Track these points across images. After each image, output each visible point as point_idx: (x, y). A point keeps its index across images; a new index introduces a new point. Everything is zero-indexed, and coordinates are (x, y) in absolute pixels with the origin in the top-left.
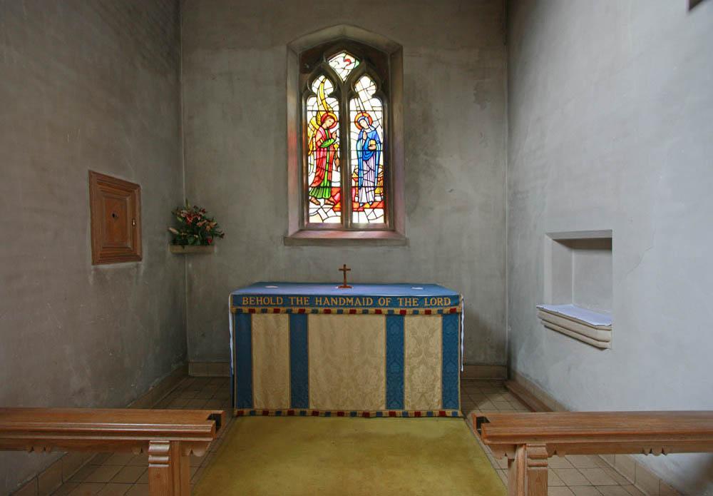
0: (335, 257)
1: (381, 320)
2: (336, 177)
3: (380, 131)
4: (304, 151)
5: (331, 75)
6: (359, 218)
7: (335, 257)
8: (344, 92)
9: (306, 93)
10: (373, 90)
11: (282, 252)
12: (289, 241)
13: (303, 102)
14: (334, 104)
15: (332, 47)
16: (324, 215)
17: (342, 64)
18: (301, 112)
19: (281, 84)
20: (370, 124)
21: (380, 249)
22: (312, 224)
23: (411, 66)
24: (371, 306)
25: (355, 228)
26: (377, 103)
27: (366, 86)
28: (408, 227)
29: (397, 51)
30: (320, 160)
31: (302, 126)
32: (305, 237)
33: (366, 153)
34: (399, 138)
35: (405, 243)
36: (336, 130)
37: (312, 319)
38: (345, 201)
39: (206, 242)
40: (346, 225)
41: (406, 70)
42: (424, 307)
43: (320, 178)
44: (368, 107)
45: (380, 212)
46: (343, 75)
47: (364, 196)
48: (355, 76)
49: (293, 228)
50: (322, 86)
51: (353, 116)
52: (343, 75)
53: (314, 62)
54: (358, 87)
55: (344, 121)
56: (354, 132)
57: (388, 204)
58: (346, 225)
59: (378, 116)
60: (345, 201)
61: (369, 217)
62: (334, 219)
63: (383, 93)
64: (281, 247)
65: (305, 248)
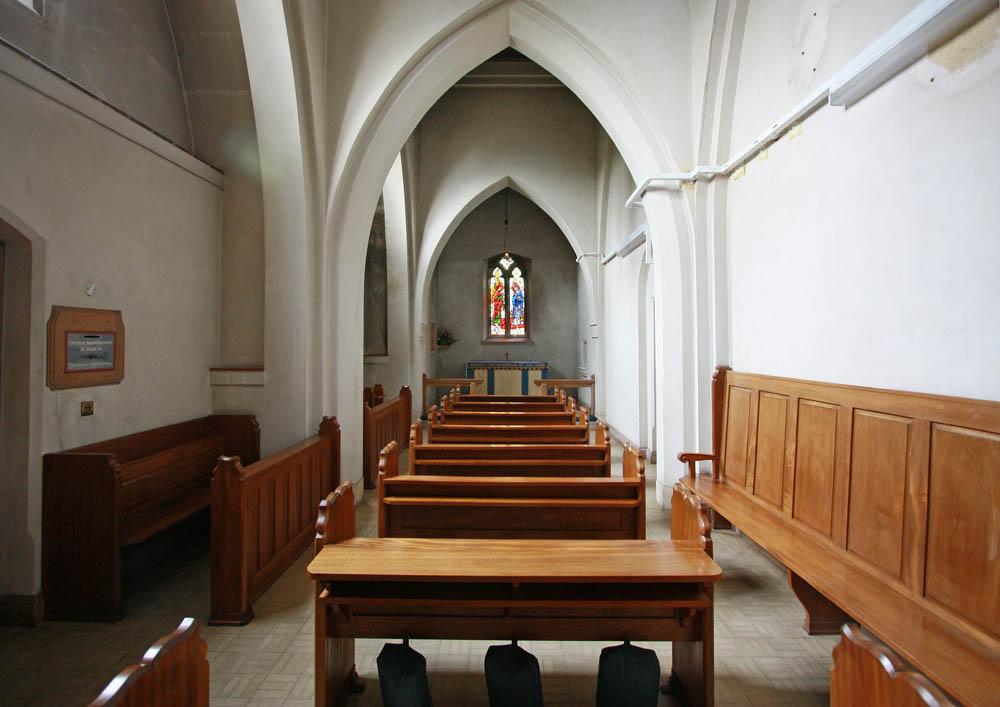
0: (502, 350)
1: (520, 372)
2: (503, 314)
3: (523, 293)
4: (489, 302)
5: (501, 268)
6: (513, 332)
7: (502, 350)
8: (507, 275)
9: (490, 276)
10: (520, 274)
11: (481, 348)
12: (483, 343)
13: (485, 281)
14: (502, 280)
15: (502, 256)
16: (497, 330)
17: (506, 263)
18: (488, 284)
19: (481, 276)
20: (519, 288)
21: (522, 347)
22: (354, 642)
23: (536, 267)
24: (517, 367)
25: (511, 337)
26: (522, 279)
27: (517, 272)
28: (535, 337)
29: (530, 260)
30: (496, 306)
31: (489, 290)
32: (491, 341)
33: (517, 302)
34: (530, 298)
35: (533, 343)
36: (503, 292)
37: (496, 371)
38: (507, 325)
39: (449, 344)
40: (508, 335)
41: (533, 268)
42: (535, 367)
43: (496, 314)
44: (518, 281)
45: (523, 329)
46: (507, 267)
47: (516, 322)
48: (512, 268)
49: (485, 338)
50: (497, 272)
51: (511, 285)
52: (507, 267)
53: (494, 263)
54: (513, 273)
55: (507, 288)
56: (512, 293)
57: (526, 326)
58: (508, 335)
59: (522, 285)
60: (507, 325)
61: (519, 332)
62: (502, 332)
63: (524, 275)
64: (481, 347)
65: (261, 599)
